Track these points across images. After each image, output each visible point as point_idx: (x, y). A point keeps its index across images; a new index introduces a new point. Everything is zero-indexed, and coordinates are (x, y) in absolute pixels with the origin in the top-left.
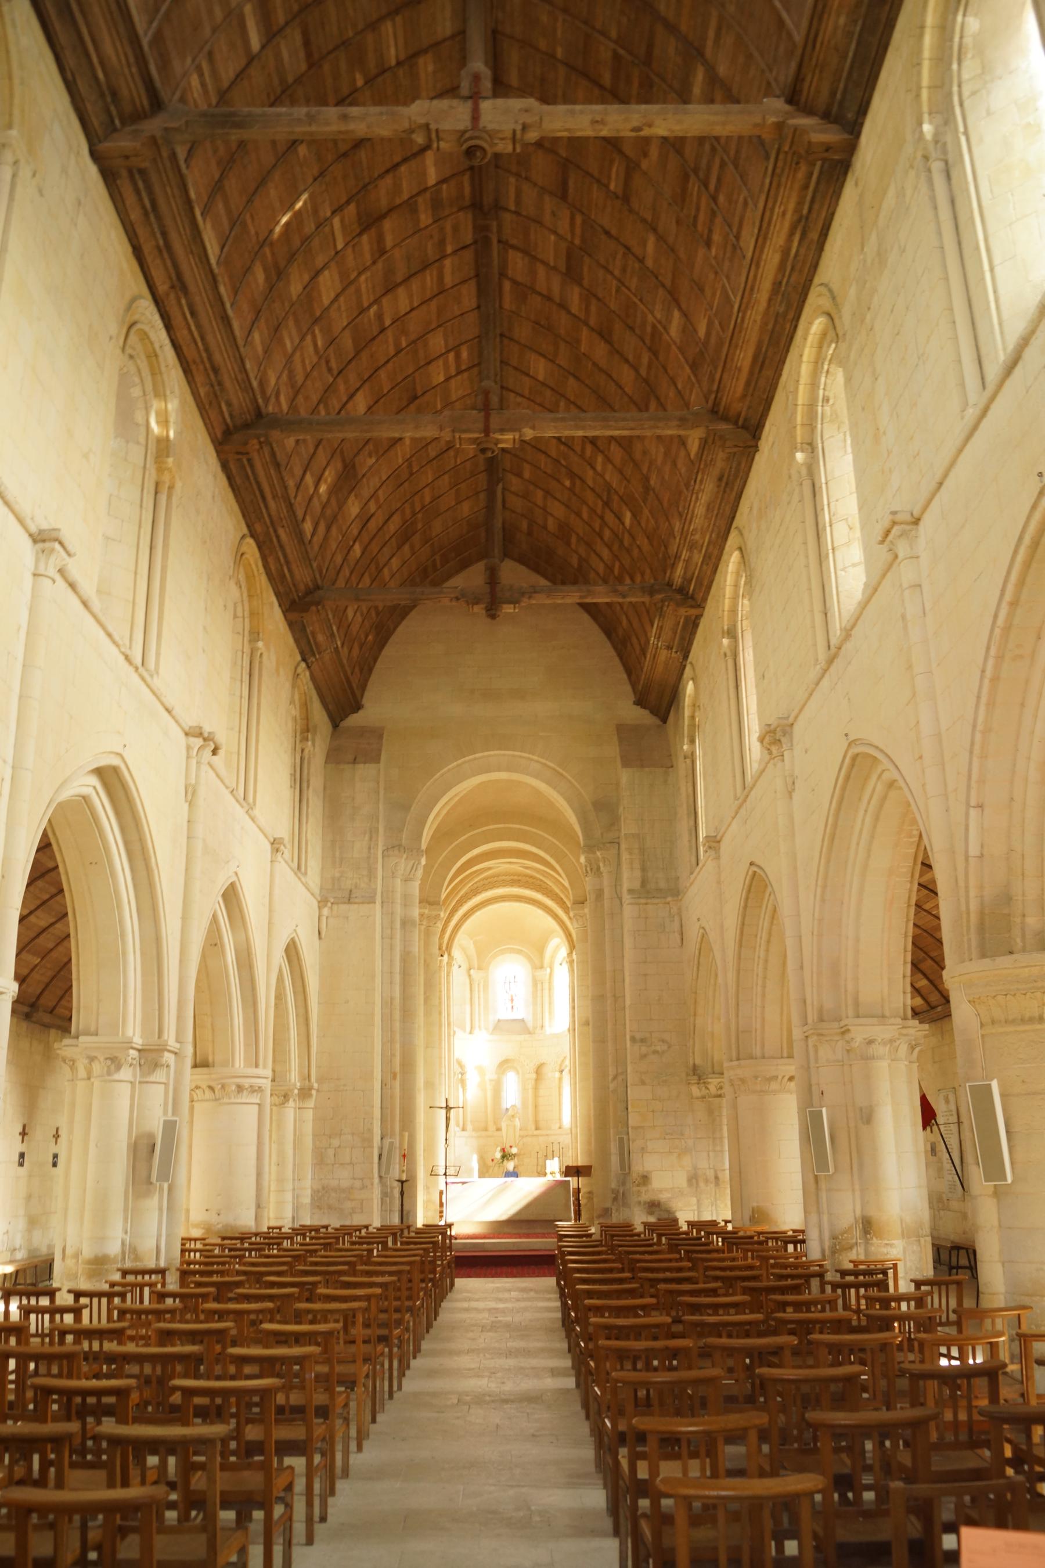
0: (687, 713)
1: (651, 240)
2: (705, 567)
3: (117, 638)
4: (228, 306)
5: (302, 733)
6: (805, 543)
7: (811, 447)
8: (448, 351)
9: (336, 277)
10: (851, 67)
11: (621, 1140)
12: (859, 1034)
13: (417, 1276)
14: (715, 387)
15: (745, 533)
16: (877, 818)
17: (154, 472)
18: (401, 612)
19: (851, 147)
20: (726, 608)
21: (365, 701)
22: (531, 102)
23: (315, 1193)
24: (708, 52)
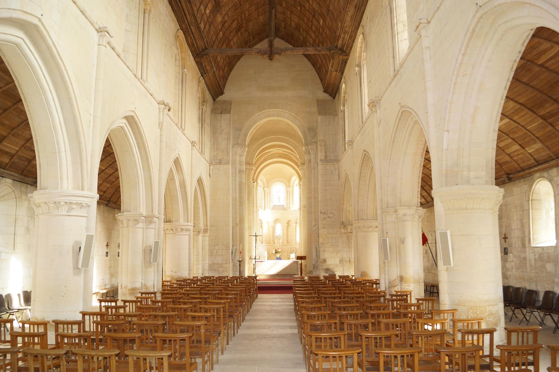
3: (131, 68)
11: (316, 248)
12: (401, 212)
13: (243, 294)
15: (365, 27)
16: (410, 135)
17: (143, 5)
18: (238, 58)
21: (225, 91)
23: (210, 265)
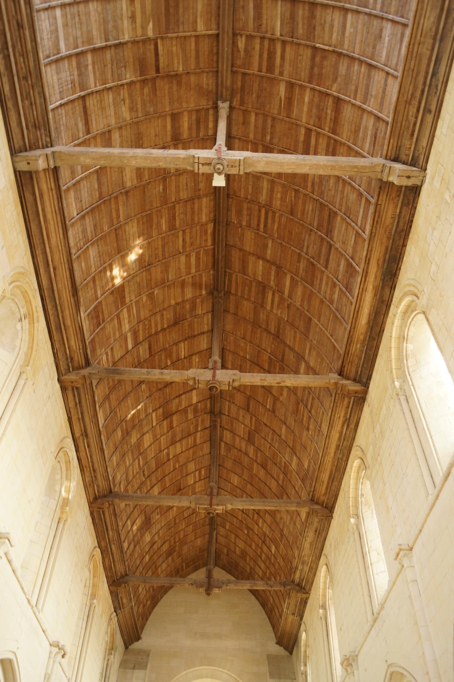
0: (303, 649)
1: (284, 427)
2: (310, 573)
3: (26, 590)
4: (104, 444)
5: (109, 650)
6: (358, 561)
7: (357, 516)
8: (196, 471)
9: (151, 437)
10: (363, 362)
14: (312, 490)
15: (329, 557)
17: (59, 513)
18: (164, 590)
19: (365, 392)
20: (321, 594)
21: (143, 636)
22: (237, 372)
24: (306, 358)
